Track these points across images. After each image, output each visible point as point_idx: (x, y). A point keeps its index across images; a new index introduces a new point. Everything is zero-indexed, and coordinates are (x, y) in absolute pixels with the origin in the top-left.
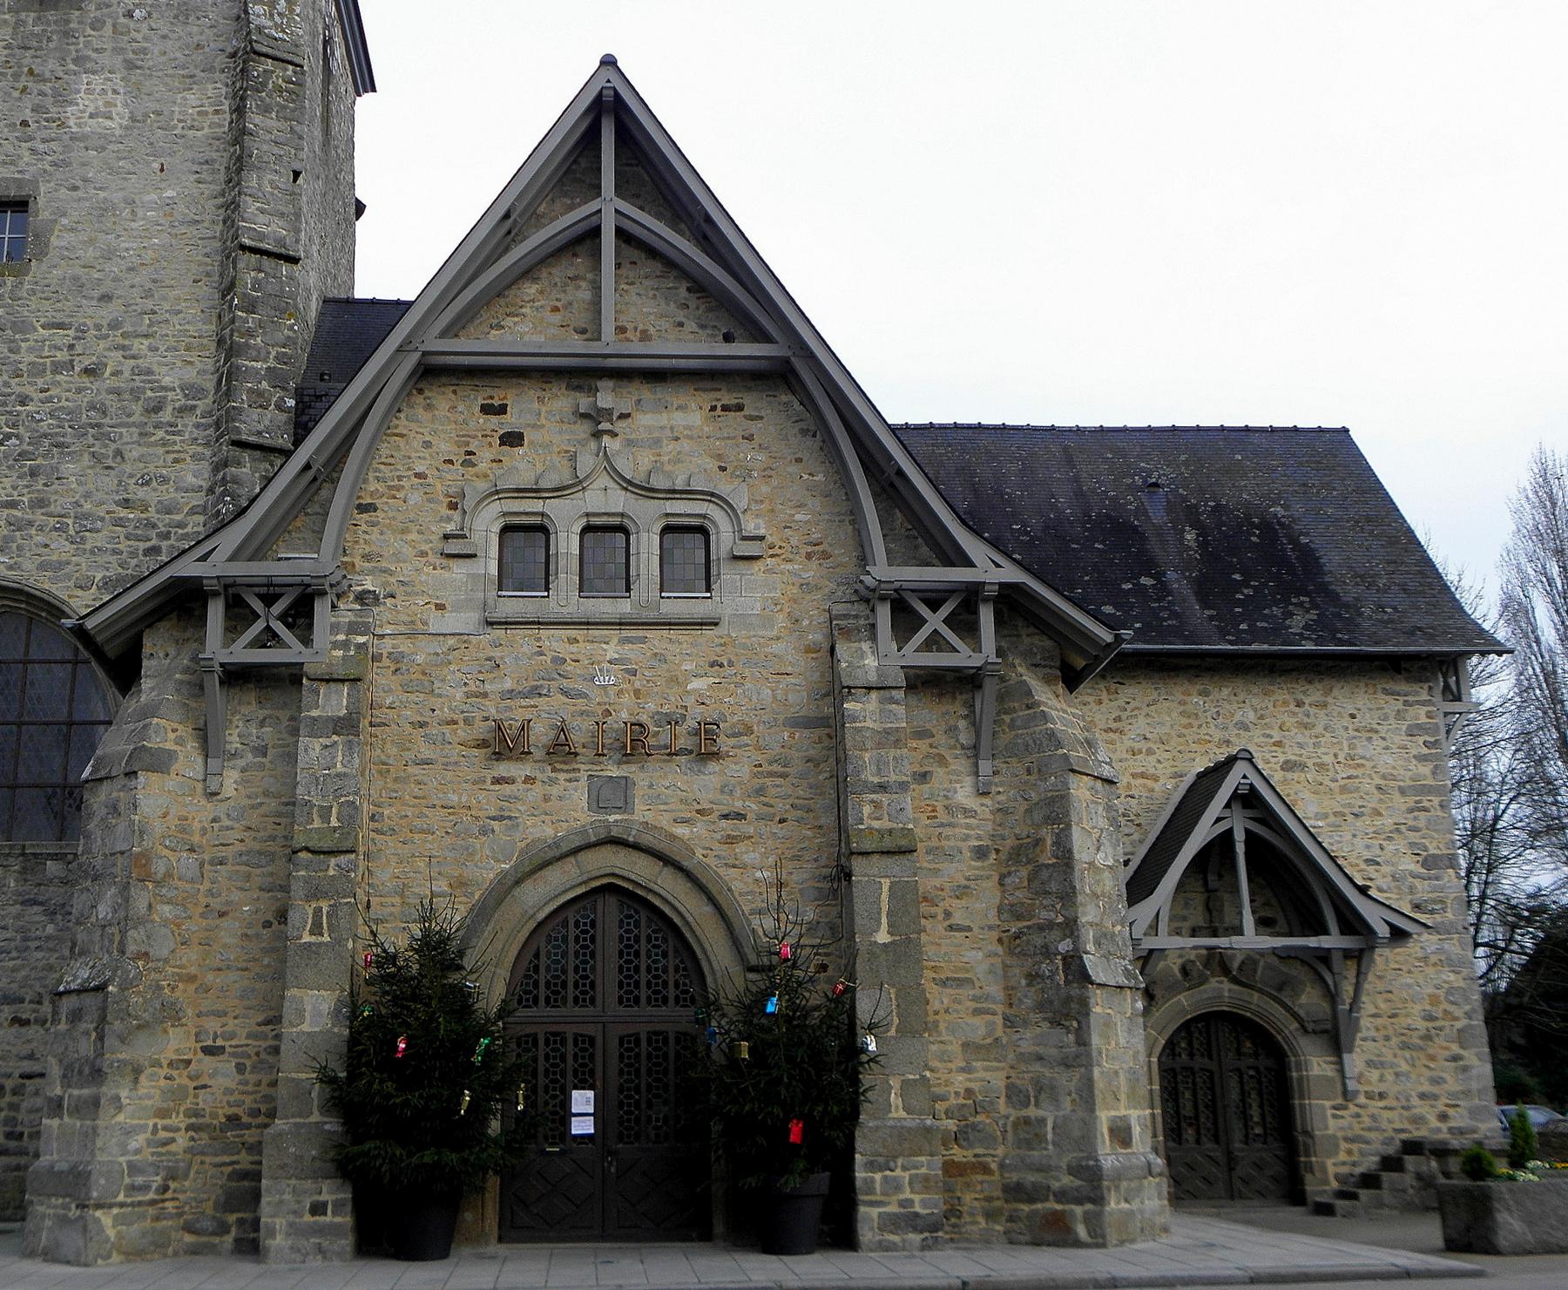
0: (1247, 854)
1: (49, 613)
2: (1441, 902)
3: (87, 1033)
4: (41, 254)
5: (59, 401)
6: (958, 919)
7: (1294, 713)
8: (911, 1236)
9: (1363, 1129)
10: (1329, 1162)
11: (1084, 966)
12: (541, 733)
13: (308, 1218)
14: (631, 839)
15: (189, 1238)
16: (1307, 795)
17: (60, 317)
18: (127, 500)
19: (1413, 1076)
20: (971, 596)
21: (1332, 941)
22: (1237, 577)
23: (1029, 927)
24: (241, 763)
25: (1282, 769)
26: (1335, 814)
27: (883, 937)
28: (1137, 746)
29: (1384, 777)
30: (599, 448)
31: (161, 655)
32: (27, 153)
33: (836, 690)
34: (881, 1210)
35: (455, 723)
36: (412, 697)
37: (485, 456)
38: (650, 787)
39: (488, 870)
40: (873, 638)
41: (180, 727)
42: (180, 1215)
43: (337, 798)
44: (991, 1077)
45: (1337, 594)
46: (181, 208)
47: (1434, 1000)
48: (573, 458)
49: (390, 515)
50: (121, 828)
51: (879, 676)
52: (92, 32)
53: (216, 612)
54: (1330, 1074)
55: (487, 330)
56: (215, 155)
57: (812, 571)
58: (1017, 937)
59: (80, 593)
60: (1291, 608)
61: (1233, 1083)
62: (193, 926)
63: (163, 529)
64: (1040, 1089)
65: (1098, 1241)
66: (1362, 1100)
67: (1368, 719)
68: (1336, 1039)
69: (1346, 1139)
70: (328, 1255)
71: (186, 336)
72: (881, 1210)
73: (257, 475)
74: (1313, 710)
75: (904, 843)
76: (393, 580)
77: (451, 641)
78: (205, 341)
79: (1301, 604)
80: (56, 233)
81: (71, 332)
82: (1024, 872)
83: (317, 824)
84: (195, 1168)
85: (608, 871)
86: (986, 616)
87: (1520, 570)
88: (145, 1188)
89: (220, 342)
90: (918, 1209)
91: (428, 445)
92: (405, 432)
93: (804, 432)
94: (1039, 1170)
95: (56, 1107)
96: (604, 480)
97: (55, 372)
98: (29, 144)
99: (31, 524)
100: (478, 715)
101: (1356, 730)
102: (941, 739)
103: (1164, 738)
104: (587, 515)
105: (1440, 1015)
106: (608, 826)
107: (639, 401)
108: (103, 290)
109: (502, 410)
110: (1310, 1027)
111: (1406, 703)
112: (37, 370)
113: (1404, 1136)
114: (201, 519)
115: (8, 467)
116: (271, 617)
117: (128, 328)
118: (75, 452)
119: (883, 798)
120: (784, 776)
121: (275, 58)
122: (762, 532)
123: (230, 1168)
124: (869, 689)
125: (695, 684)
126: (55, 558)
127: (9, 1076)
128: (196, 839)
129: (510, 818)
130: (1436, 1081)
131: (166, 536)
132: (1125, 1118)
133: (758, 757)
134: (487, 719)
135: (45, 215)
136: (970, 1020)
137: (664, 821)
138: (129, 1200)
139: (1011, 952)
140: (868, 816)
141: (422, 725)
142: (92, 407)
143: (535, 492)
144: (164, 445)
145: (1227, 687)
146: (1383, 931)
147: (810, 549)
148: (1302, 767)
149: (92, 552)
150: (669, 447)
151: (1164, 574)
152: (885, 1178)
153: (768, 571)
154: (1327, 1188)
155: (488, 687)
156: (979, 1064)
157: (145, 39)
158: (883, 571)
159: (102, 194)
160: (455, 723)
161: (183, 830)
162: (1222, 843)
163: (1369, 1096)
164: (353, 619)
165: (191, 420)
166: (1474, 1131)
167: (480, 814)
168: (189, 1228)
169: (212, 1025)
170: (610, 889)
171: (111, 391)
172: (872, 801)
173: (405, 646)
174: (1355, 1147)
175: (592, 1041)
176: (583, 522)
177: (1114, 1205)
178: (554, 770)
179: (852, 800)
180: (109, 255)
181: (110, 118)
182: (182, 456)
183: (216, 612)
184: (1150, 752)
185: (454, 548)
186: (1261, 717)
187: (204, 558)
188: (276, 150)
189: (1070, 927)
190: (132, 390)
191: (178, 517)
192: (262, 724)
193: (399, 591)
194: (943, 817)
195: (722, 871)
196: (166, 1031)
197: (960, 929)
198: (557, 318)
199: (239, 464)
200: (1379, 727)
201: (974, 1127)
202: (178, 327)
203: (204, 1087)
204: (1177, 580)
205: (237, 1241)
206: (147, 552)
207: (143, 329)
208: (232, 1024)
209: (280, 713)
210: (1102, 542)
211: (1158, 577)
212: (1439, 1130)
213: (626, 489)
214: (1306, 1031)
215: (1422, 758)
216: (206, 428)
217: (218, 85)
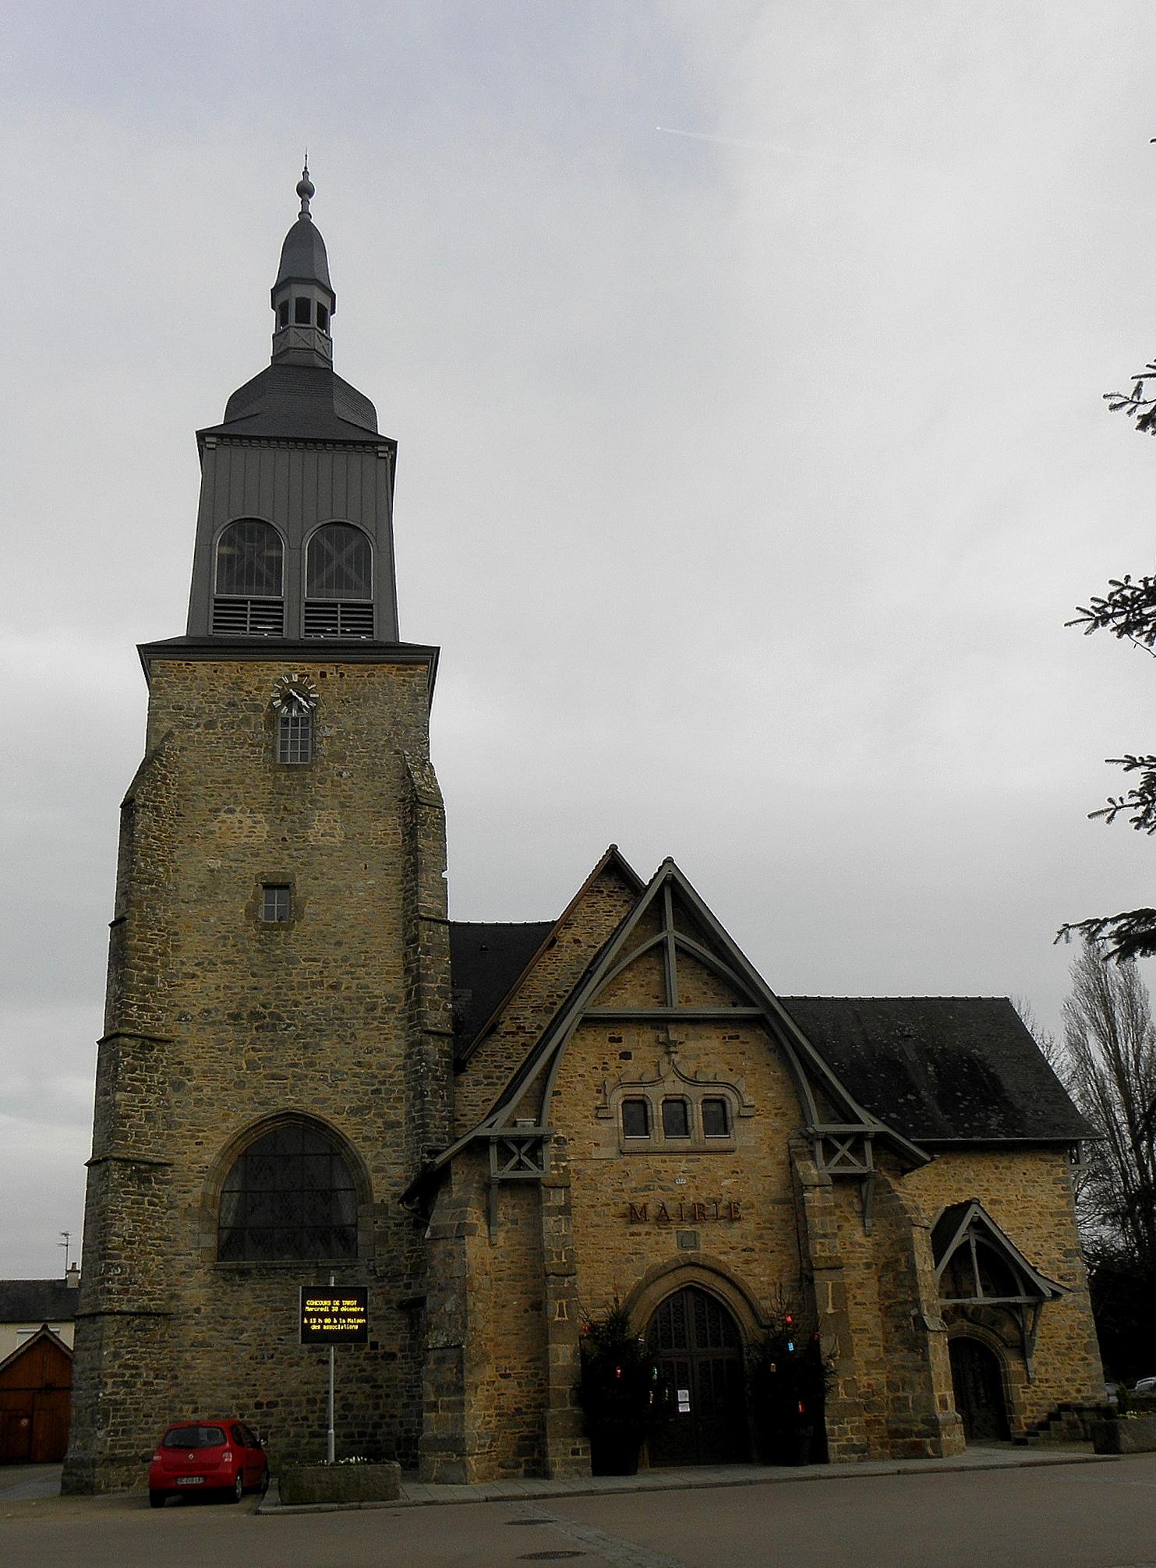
0: (976, 1253)
1: (316, 1126)
2: (1073, 1274)
3: (450, 1369)
4: (300, 918)
5: (317, 1004)
6: (859, 1299)
7: (994, 1172)
8: (853, 1455)
9: (1038, 1399)
10: (1022, 1417)
11: (924, 1322)
12: (652, 1210)
13: (571, 1457)
14: (701, 1263)
15: (501, 1470)
16: (1003, 1218)
18: (359, 1062)
19: (1063, 1369)
20: (860, 1137)
21: (1021, 1299)
22: (959, 1094)
23: (895, 1303)
24: (506, 1228)
25: (989, 1203)
26: (1018, 1228)
27: (830, 1310)
30: (670, 1060)
31: (461, 1172)
32: (287, 857)
33: (795, 1188)
34: (839, 1443)
35: (609, 1205)
36: (588, 1192)
37: (613, 1064)
38: (707, 1235)
39: (631, 1280)
40: (813, 1158)
41: (477, 1211)
42: (497, 1458)
43: (564, 1247)
44: (880, 1377)
45: (1012, 1103)
46: (378, 891)
47: (1072, 1328)
48: (658, 1065)
49: (569, 1097)
50: (456, 1265)
51: (820, 1179)
52: (320, 786)
53: (493, 1151)
54: (1020, 1369)
55: (608, 997)
56: (395, 860)
57: (777, 1123)
58: (888, 1307)
59: (338, 1116)
60: (989, 1113)
63: (381, 1079)
64: (904, 1384)
65: (939, 1455)
66: (1037, 1383)
67: (1033, 1175)
68: (1023, 1350)
69: (1030, 1405)
70: (582, 1474)
71: (386, 966)
72: (839, 1443)
73: (437, 1049)
74: (1003, 1171)
75: (837, 1263)
76: (572, 1131)
77: (604, 1162)
78: (397, 969)
79: (994, 1110)
80: (308, 905)
82: (891, 1275)
83: (555, 1260)
84: (501, 1435)
85: (691, 1279)
86: (868, 1147)
87: (1075, 1015)
88: (484, 1446)
89: (407, 971)
90: (855, 1442)
91: (584, 1059)
92: (572, 1052)
93: (770, 1050)
94: (907, 1422)
95: (433, 1407)
96: (673, 1077)
97: (313, 987)
98: (287, 852)
99: (306, 1076)
101: (1027, 1181)
102: (846, 1208)
103: (927, 1188)
104: (666, 1095)
105: (1075, 1336)
106: (689, 1257)
107: (686, 1035)
108: (337, 938)
109: (619, 1040)
110: (1009, 1344)
111: (1051, 1166)
113: (1059, 1402)
114: (403, 1073)
115: (291, 1043)
116: (521, 1154)
117: (352, 961)
118: (329, 1034)
119: (826, 1241)
120: (771, 1229)
121: (430, 806)
122: (752, 1103)
123: (519, 1435)
124: (815, 1186)
125: (725, 1183)
126: (321, 1096)
127: (318, 1392)
128: (488, 1268)
129: (640, 1253)
130: (1074, 1372)
131: (383, 1083)
132: (944, 1395)
133: (758, 1220)
134: (624, 1203)
135: (300, 894)
136: (867, 1349)
137: (715, 1253)
138: (479, 1452)
139: (886, 1315)
140: (819, 1250)
141: (593, 1206)
143: (639, 1083)
144: (378, 1030)
145: (958, 1159)
146: (1049, 1294)
147: (776, 1111)
148: (1000, 1202)
149: (342, 1092)
150: (704, 1059)
151: (919, 1093)
152: (839, 1428)
153: (758, 1123)
154: (1021, 1430)
156: (873, 1371)
157: (350, 790)
158: (819, 1127)
159: (333, 882)
160: (609, 1205)
161: (483, 1264)
162: (964, 1248)
164: (556, 1152)
166: (1094, 1398)
167: (625, 1252)
168: (501, 1465)
169: (504, 1363)
170: (689, 1288)
172: (821, 1243)
173: (581, 1166)
175: (686, 1364)
176: (664, 1098)
178: (659, 1228)
179: (811, 1242)
180: (339, 918)
181: (334, 837)
182: (389, 1036)
183: (493, 1151)
185: (601, 1113)
186: (978, 1176)
187: (491, 1126)
188: (434, 860)
189: (916, 1303)
190: (358, 997)
192: (514, 1207)
193: (576, 1137)
195: (744, 1278)
196: (484, 1367)
198: (643, 990)
199: (428, 1044)
200: (1038, 1180)
201: (872, 1402)
202: (381, 961)
203: (503, 1394)
204: (928, 1097)
205: (526, 1471)
206: (373, 1092)
207: (360, 962)
208: (513, 1363)
209: (522, 1202)
210: (884, 1073)
211: (917, 1094)
212: (1077, 1398)
213: (684, 1081)
214: (1007, 1347)
215: (1061, 1196)
216: (401, 1019)
217: (395, 818)
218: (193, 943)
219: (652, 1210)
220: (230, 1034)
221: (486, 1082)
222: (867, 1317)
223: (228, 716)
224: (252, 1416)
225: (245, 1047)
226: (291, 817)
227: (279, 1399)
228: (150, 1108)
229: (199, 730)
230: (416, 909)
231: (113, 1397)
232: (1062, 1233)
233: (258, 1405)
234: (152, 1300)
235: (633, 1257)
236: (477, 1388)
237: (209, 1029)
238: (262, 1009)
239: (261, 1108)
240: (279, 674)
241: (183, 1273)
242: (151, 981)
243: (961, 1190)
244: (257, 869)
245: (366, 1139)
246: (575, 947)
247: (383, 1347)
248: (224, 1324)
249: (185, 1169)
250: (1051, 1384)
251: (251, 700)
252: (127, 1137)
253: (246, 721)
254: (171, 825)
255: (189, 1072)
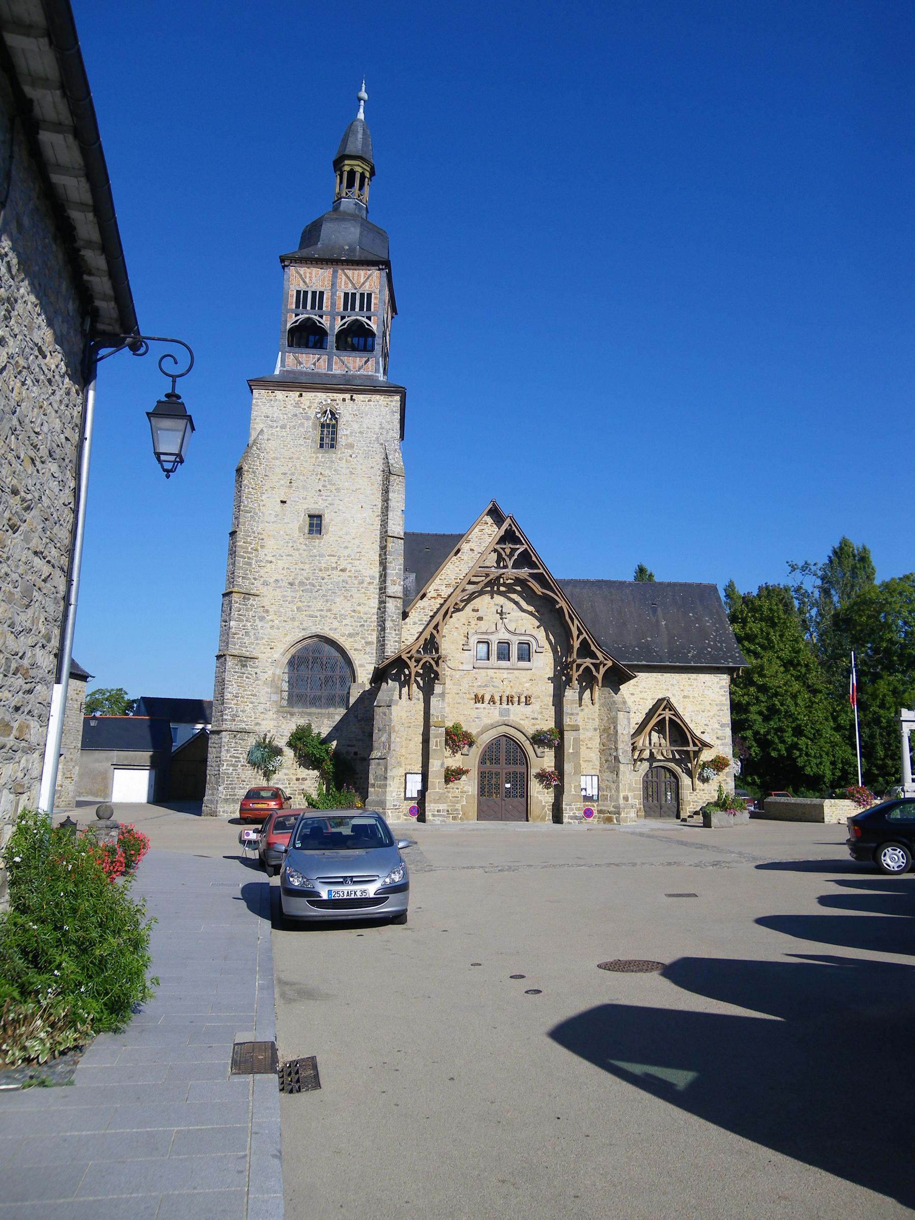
6: (589, 745)
10: (688, 808)
12: (487, 698)
16: (689, 705)
17: (333, 553)
27: (571, 751)
28: (642, 690)
29: (712, 701)
32: (320, 500)
36: (455, 687)
56: (377, 503)
59: (341, 637)
61: (663, 785)
62: (404, 743)
64: (607, 788)
66: (697, 791)
74: (693, 681)
77: (465, 672)
81: (336, 558)
91: (459, 620)
95: (373, 785)
99: (327, 616)
100: (472, 692)
112: (327, 569)
113: (709, 801)
117: (353, 557)
119: (572, 717)
131: (366, 621)
137: (518, 720)
141: (458, 694)
142: (343, 581)
143: (486, 633)
153: (545, 656)
155: (474, 684)
159: (344, 515)
163: (700, 790)
165: (372, 587)
171: (349, 576)
174: (695, 804)
177: (622, 815)
184: (646, 692)
191: (370, 616)
194: (586, 720)
197: (589, 748)
207: (357, 558)
218: (270, 544)
219: (487, 698)
220: (289, 593)
221: (419, 623)
222: (593, 755)
223: (293, 422)
224: (294, 784)
225: (296, 600)
226: (324, 478)
227: (308, 777)
228: (248, 629)
229: (278, 429)
230: (386, 532)
231: (227, 771)
232: (721, 714)
233: (298, 779)
234: (247, 725)
235: (476, 719)
236: (394, 778)
237: (278, 590)
238: (305, 581)
239: (303, 631)
240: (320, 399)
241: (262, 713)
242: (250, 564)
243: (668, 690)
244: (305, 506)
245: (355, 650)
246: (471, 552)
247: (360, 754)
248: (282, 739)
249: (265, 661)
250: (706, 792)
251: (305, 413)
252: (235, 644)
253: (302, 425)
254: (262, 482)
255: (267, 611)
